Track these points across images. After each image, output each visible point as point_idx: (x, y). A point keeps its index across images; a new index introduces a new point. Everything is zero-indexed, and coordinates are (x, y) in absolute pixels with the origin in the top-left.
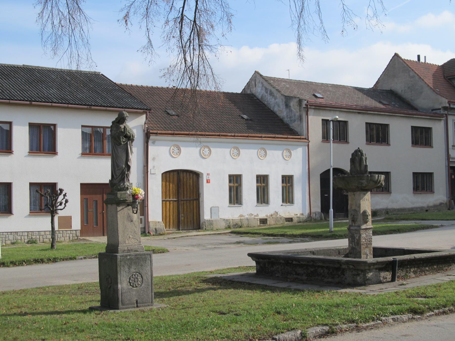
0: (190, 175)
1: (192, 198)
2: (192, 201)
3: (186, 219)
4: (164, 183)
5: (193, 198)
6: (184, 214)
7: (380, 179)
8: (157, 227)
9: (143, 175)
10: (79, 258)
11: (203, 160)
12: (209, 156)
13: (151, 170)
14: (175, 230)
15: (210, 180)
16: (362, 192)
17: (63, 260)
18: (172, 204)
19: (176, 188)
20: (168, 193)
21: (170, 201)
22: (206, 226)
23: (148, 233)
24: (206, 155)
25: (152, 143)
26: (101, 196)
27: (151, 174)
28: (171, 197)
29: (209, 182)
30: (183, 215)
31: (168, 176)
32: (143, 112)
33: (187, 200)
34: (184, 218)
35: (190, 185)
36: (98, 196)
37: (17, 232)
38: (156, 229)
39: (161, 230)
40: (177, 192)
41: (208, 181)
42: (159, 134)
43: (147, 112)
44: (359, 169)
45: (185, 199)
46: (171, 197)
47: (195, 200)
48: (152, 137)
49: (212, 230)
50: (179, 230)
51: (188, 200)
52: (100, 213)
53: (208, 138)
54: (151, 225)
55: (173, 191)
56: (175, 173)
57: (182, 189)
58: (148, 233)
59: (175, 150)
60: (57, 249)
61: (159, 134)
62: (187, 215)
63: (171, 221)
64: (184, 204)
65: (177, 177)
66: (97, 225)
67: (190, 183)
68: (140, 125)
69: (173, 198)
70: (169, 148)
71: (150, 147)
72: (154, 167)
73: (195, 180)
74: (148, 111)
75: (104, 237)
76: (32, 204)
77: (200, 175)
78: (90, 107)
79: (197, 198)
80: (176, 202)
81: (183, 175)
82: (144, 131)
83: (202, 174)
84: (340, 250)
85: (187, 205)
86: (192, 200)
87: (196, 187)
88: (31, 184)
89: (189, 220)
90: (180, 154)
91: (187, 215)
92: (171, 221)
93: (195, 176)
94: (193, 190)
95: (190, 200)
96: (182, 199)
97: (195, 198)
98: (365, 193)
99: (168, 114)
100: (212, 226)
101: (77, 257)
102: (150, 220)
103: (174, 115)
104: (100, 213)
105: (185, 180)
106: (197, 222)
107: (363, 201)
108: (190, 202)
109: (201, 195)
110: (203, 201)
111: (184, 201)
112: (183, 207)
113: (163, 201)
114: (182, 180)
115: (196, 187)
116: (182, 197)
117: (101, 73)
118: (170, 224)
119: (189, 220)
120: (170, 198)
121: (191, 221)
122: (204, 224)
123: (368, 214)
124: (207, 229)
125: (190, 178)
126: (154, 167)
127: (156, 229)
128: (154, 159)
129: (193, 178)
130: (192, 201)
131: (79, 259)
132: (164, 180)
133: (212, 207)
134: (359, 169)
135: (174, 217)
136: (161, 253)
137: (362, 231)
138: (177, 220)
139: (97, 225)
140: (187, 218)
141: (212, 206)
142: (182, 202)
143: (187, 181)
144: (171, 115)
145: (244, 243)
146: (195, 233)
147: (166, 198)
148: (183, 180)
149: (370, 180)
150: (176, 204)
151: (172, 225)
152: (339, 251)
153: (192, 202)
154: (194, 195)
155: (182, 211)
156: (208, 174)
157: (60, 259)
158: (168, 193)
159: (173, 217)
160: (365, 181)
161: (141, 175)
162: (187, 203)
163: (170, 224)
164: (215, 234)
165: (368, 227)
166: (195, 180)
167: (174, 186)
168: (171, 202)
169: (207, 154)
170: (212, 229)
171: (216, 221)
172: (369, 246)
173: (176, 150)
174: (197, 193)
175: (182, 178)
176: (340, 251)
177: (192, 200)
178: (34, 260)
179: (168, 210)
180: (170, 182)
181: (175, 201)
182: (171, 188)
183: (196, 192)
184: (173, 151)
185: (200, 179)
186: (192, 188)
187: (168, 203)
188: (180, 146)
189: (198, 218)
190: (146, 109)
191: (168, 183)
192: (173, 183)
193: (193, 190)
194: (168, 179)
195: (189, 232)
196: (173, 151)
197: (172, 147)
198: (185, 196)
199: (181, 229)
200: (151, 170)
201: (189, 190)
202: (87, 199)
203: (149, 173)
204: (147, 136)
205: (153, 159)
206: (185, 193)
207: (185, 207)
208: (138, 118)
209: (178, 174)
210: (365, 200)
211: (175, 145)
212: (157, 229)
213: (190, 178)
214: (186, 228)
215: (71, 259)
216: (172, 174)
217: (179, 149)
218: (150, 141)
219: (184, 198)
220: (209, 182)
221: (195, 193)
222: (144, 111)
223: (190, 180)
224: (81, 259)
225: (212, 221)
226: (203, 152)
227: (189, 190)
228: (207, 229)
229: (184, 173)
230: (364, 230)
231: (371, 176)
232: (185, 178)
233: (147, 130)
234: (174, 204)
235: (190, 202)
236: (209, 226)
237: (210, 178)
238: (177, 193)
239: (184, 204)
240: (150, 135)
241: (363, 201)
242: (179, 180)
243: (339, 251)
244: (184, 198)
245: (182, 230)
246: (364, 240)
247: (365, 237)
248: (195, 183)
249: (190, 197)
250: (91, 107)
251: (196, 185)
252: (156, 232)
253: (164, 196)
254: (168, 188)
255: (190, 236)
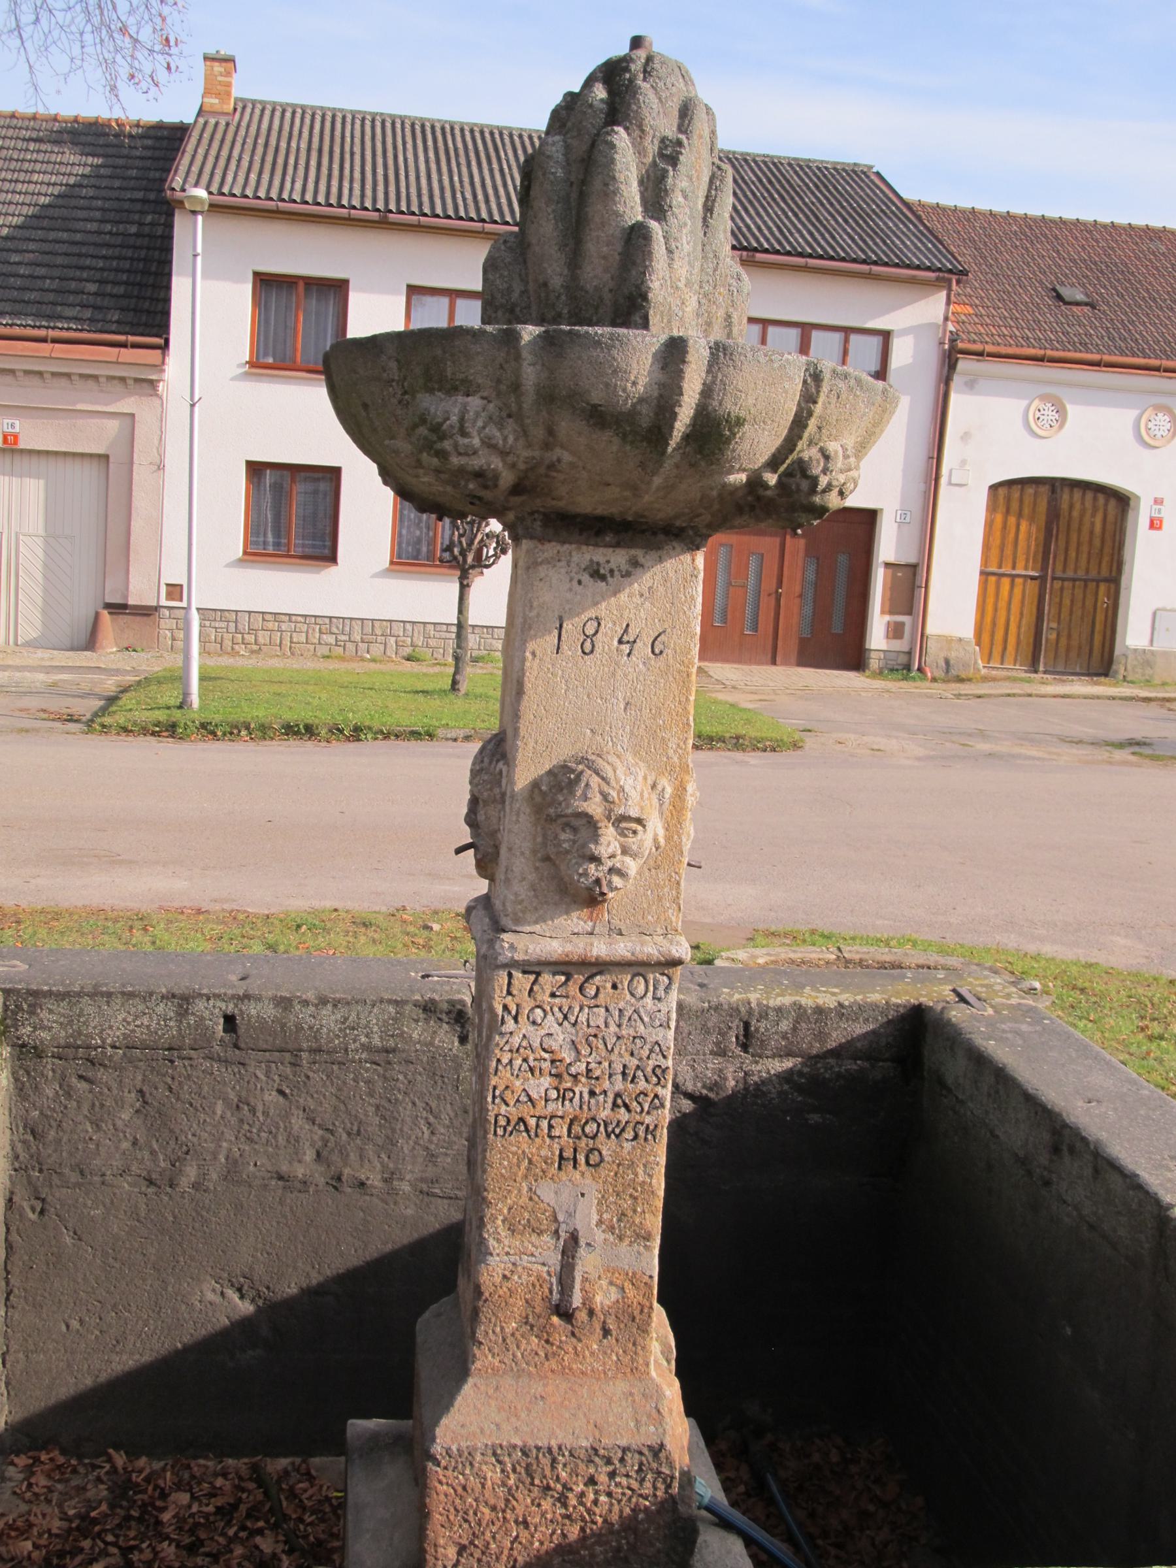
0: (1095, 499)
1: (1093, 574)
2: (1094, 584)
3: (1063, 641)
4: (999, 518)
5: (1099, 573)
6: (1059, 623)
7: (707, 392)
8: (953, 655)
9: (922, 487)
10: (449, 736)
11: (1147, 453)
12: (1169, 442)
13: (951, 471)
14: (1020, 672)
15: (1161, 522)
16: (551, 549)
17: (386, 737)
18: (1021, 587)
19: (1042, 537)
20: (1009, 551)
21: (1013, 577)
22: (1129, 667)
23: (920, 669)
24: (1159, 435)
25: (966, 384)
26: (778, 540)
27: (950, 484)
28: (1021, 563)
29: (1160, 528)
30: (1054, 625)
31: (1016, 495)
32: (938, 279)
33: (1074, 580)
34: (1058, 635)
35: (1092, 533)
36: (768, 539)
37: (493, 627)
38: (947, 662)
39: (966, 665)
40: (1041, 549)
41: (1155, 524)
42: (989, 355)
43: (950, 281)
44: (556, 282)
45: (1070, 574)
46: (1021, 563)
47: (1107, 580)
48: (964, 365)
49: (1148, 683)
50: (1036, 672)
51: (1080, 580)
52: (769, 595)
53: (1170, 378)
54: (932, 647)
55: (1029, 547)
56: (1044, 490)
57: (1062, 543)
58: (920, 669)
59: (1046, 413)
60: (467, 694)
61: (989, 355)
62: (1070, 630)
63: (1012, 640)
64: (1062, 589)
65: (1049, 503)
66: (755, 629)
67: (1093, 524)
68: (930, 325)
69: (1026, 568)
70: (1024, 403)
71: (954, 398)
72: (963, 462)
73: (1111, 518)
74: (954, 278)
75: (774, 668)
76: (253, 529)
77: (1132, 503)
78: (750, 254)
79: (1114, 574)
80: (1037, 582)
81: (1071, 497)
82: (942, 343)
83: (1138, 498)
84: (764, 1014)
85: (1073, 594)
86: (1093, 580)
87: (1114, 542)
88: (255, 469)
89: (1075, 643)
90: (1061, 427)
91: (1070, 630)
92: (1012, 640)
93: (1113, 503)
94: (1102, 550)
95: (1085, 581)
96: (1059, 574)
97: (1105, 573)
98: (618, 558)
99: (1059, 297)
100: (1148, 671)
101: (440, 732)
102: (930, 630)
103: (1078, 304)
104: (769, 595)
105: (1075, 514)
106: (1103, 652)
107: (571, 648)
108: (1086, 586)
109: (1126, 568)
110: (1129, 588)
111: (1063, 580)
112: (1057, 600)
113: (984, 574)
114: (1066, 514)
115: (1114, 542)
116: (1059, 567)
117: (875, 170)
118: (1005, 649)
119: (1075, 643)
120: (1014, 568)
121: (1080, 647)
122: (1123, 662)
123: (595, 807)
124: (1129, 679)
125: (1095, 510)
126: (963, 462)
127: (947, 662)
128: (965, 437)
129: (1105, 510)
130: (1094, 584)
131: (447, 739)
132: (1002, 508)
133: (1159, 609)
134: (556, 282)
135: (1023, 630)
136: (765, 751)
137: (522, 981)
138: (1031, 640)
139: (755, 629)
140: (1069, 636)
141: (1160, 605)
142: (1058, 584)
143: (1082, 516)
144: (1066, 303)
145: (1146, 751)
146: (1080, 687)
147: (1000, 567)
148: (1070, 513)
149: (549, 397)
150: (1033, 587)
151: (1013, 653)
152: (747, 1025)
153: (1092, 585)
154: (1104, 564)
155: (1053, 611)
156: (1158, 501)
157: (376, 733)
158: (1009, 551)
159: (1019, 627)
160: (475, 402)
161: (918, 487)
162: (1074, 587)
163: (1005, 649)
164: (1131, 699)
165: (600, 949)
166: (1111, 518)
167: (1034, 529)
168: (1019, 581)
169: (1161, 432)
170: (1148, 681)
171: (1165, 654)
172: (607, 1148)
173: (1050, 414)
174: (1116, 557)
175: (1065, 506)
176: (761, 1026)
177: (1093, 580)
178: (283, 727)
179: (1002, 604)
180: (1020, 515)
181: (1033, 578)
182: (1022, 536)
183: (1113, 555)
184: (1038, 414)
185: (1131, 514)
186: (1097, 542)
187: (1006, 582)
188: (1065, 402)
189: (1108, 638)
190: (950, 271)
191: (1012, 520)
192: (1032, 519)
193: (1102, 550)
194: (1015, 505)
195: (1064, 681)
196: (1038, 414)
197: (1036, 403)
198: (1071, 565)
199: (1041, 668)
200: (951, 471)
201: (1085, 548)
202: (732, 546)
203: (943, 481)
204: (950, 360)
205: (962, 438)
206: (1073, 554)
207: (1067, 602)
208: (922, 303)
209: (1053, 491)
210: (607, 640)
211: (1044, 398)
212: (952, 662)
213: (1095, 510)
214: (1060, 668)
215: (415, 735)
216: (1030, 490)
217: (1061, 411)
218: (956, 377)
219: (1064, 571)
220: (1160, 528)
221: (1106, 559)
222: (941, 274)
223: (1093, 515)
224: (455, 740)
225: (1153, 653)
226: (1146, 425)
227: (1085, 548)
228: (1129, 679)
229: (1076, 490)
230: (549, 981)
231: (549, 341)
232: (1078, 506)
233: (953, 341)
234: (1028, 587)
235: (1086, 586)
236: (1140, 671)
237: (1165, 513)
238: (1044, 552)
239: (1062, 589)
240: (957, 359)
241: (571, 648)
242: (1053, 515)
243: (747, 1025)
244: (1064, 571)
245: (1045, 672)
246: (540, 1086)
247: (567, 1056)
248: (1109, 527)
249: (1087, 571)
250: (753, 256)
251: (1115, 535)
252: (947, 671)
253: (994, 559)
254: (1012, 535)
255: (1037, 696)
